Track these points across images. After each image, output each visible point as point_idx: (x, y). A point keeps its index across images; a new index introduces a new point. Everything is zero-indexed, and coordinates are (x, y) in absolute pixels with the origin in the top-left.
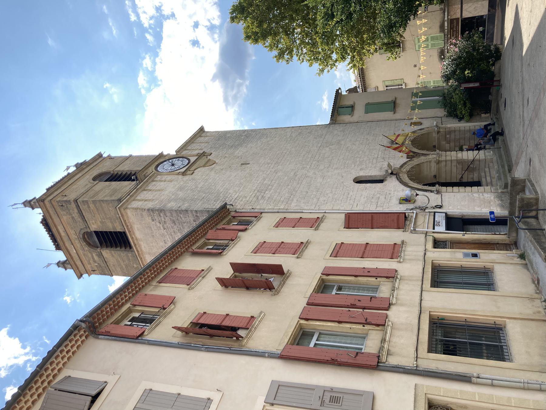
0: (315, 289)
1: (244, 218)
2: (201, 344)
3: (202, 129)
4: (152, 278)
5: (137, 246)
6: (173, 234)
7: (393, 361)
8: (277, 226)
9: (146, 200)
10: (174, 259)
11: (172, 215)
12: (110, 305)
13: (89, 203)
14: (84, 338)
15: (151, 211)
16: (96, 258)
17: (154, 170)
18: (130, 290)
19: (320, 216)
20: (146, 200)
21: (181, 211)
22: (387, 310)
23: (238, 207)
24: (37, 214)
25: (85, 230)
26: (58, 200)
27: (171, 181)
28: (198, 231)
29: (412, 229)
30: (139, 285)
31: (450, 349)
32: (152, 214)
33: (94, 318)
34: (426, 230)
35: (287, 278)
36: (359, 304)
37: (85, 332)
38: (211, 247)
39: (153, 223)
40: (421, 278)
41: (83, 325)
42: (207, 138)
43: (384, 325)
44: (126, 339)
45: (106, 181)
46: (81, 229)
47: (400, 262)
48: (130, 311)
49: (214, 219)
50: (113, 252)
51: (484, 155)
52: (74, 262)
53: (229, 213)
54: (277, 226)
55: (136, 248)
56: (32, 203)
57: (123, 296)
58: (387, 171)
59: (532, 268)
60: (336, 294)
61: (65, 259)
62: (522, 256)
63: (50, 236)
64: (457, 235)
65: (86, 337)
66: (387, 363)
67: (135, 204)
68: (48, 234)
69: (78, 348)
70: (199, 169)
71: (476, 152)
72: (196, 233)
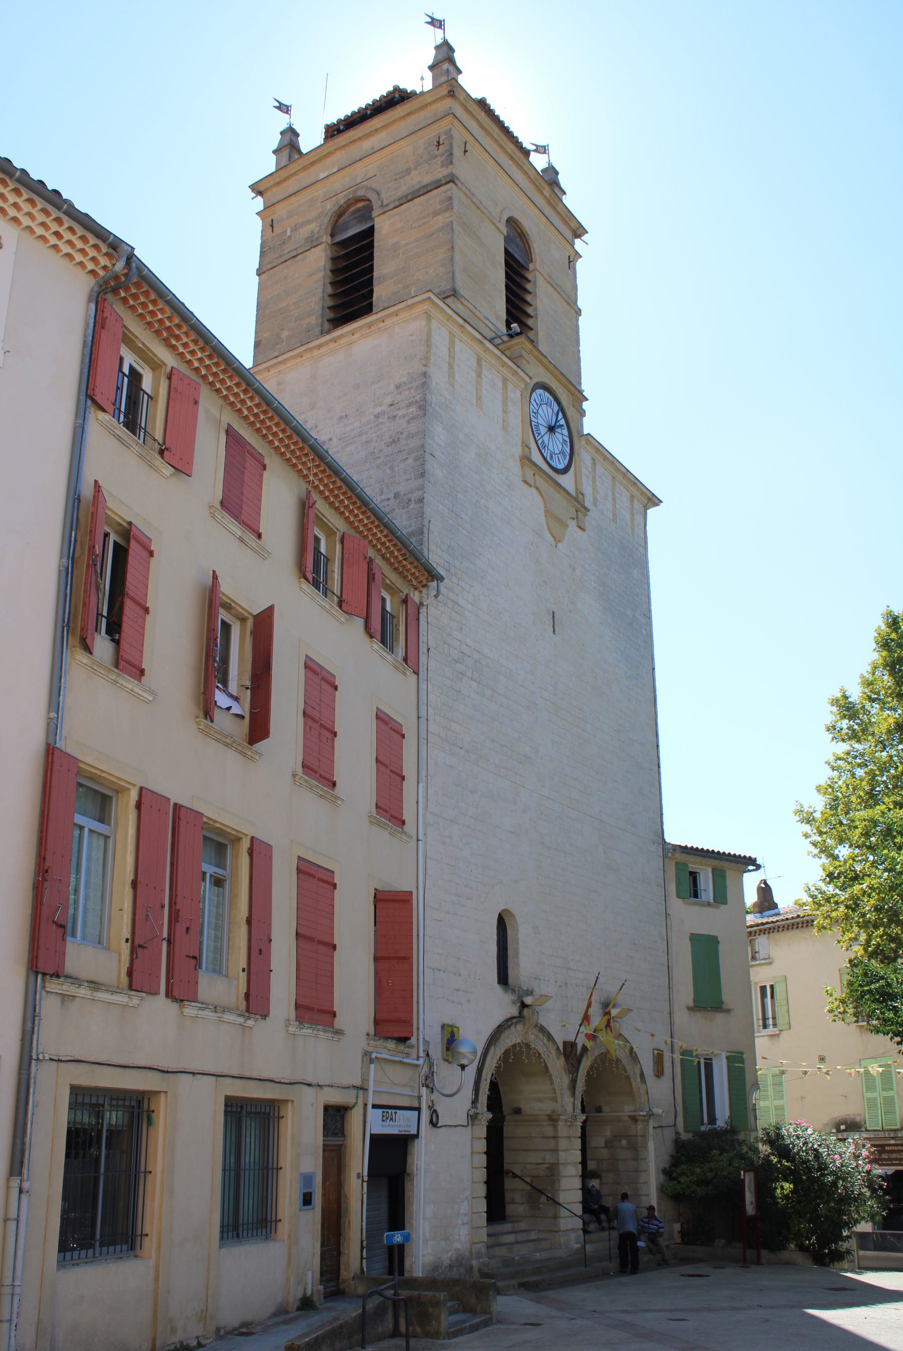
0: (215, 821)
1: (402, 628)
2: (77, 555)
3: (653, 501)
4: (239, 411)
5: (332, 345)
6: (364, 438)
7: (49, 1007)
8: (382, 718)
9: (451, 366)
10: (289, 460)
11: (411, 436)
12: (169, 318)
13: (447, 215)
14: (90, 266)
15: (424, 381)
16: (305, 231)
17: (535, 380)
18: (208, 362)
19: (409, 827)
20: (451, 366)
21: (421, 460)
22: (167, 996)
23: (432, 611)
24: (418, 79)
25: (376, 204)
26: (455, 133)
27: (505, 427)
28: (364, 513)
29: (374, 1056)
30: (222, 381)
31: (78, 1141)
32: (417, 383)
33: (137, 285)
34: (371, 1089)
35: (241, 753)
36: (180, 928)
37: (105, 268)
38: (323, 550)
39: (392, 388)
40: (248, 1075)
41: (120, 266)
42: (628, 517)
43: (131, 988)
44: (86, 370)
45: (507, 252)
46: (378, 194)
47: (286, 1026)
48: (155, 365)
49: (399, 550)
50: (320, 275)
51: (569, 1227)
52: (295, 174)
53: (416, 588)
54: (382, 718)
55: (327, 343)
56: (446, 66)
57: (192, 346)
58: (530, 993)
59: (277, 1324)
60: (204, 874)
61: (304, 150)
62: (306, 1304)
63: (360, 110)
64: (358, 1161)
65: (93, 272)
66: (44, 993)
67: (441, 337)
68: (368, 106)
69: (68, 255)
70: (539, 499)
71: (578, 1209)
72: (359, 508)
